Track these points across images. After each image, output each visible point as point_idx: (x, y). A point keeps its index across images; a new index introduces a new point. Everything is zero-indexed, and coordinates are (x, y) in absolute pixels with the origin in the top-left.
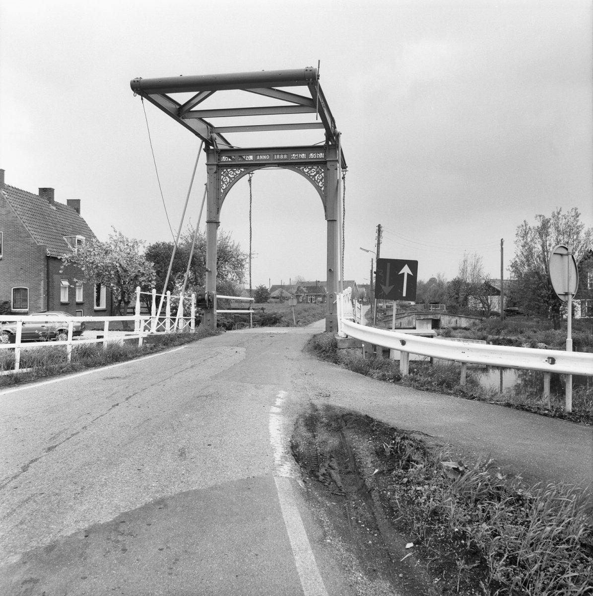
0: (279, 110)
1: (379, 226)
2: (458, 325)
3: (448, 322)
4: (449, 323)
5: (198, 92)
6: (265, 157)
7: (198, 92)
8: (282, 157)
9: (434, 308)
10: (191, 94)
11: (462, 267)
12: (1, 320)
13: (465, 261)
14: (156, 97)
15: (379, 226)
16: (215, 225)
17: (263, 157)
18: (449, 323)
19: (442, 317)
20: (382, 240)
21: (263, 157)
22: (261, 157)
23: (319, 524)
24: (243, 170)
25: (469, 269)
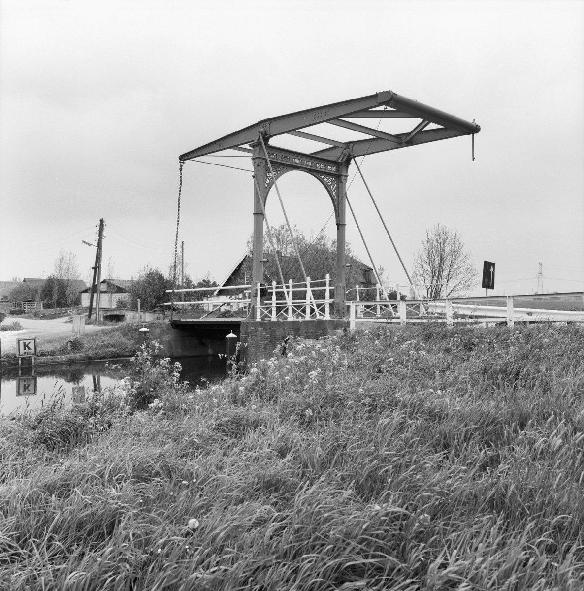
0: (360, 129)
1: (102, 221)
2: (143, 320)
3: (132, 317)
4: (134, 318)
6: (298, 161)
8: (310, 164)
9: (29, 307)
10: (426, 128)
11: (57, 265)
12: (2, 280)
13: (62, 259)
14: (330, 121)
15: (102, 221)
16: (261, 216)
17: (297, 161)
18: (134, 318)
19: (126, 313)
20: (105, 233)
21: (297, 161)
23: (459, 411)
25: (65, 267)
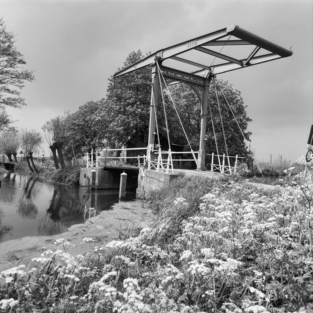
5: (271, 53)
7: (271, 53)
22: (178, 75)
24: (170, 80)
